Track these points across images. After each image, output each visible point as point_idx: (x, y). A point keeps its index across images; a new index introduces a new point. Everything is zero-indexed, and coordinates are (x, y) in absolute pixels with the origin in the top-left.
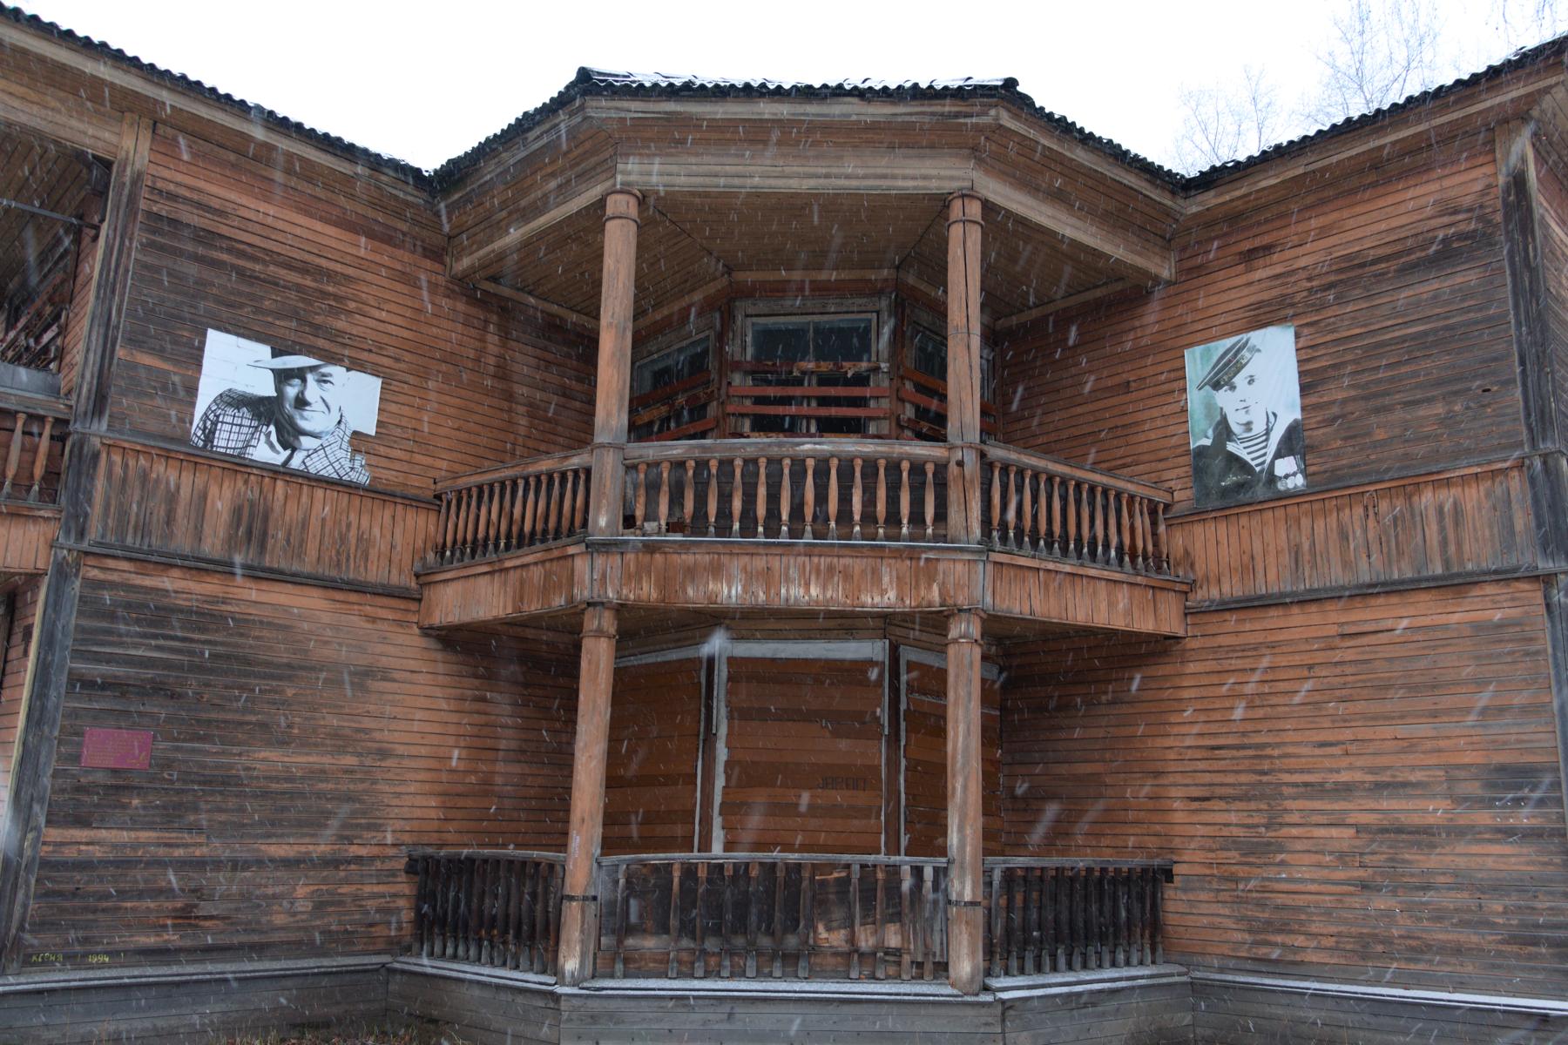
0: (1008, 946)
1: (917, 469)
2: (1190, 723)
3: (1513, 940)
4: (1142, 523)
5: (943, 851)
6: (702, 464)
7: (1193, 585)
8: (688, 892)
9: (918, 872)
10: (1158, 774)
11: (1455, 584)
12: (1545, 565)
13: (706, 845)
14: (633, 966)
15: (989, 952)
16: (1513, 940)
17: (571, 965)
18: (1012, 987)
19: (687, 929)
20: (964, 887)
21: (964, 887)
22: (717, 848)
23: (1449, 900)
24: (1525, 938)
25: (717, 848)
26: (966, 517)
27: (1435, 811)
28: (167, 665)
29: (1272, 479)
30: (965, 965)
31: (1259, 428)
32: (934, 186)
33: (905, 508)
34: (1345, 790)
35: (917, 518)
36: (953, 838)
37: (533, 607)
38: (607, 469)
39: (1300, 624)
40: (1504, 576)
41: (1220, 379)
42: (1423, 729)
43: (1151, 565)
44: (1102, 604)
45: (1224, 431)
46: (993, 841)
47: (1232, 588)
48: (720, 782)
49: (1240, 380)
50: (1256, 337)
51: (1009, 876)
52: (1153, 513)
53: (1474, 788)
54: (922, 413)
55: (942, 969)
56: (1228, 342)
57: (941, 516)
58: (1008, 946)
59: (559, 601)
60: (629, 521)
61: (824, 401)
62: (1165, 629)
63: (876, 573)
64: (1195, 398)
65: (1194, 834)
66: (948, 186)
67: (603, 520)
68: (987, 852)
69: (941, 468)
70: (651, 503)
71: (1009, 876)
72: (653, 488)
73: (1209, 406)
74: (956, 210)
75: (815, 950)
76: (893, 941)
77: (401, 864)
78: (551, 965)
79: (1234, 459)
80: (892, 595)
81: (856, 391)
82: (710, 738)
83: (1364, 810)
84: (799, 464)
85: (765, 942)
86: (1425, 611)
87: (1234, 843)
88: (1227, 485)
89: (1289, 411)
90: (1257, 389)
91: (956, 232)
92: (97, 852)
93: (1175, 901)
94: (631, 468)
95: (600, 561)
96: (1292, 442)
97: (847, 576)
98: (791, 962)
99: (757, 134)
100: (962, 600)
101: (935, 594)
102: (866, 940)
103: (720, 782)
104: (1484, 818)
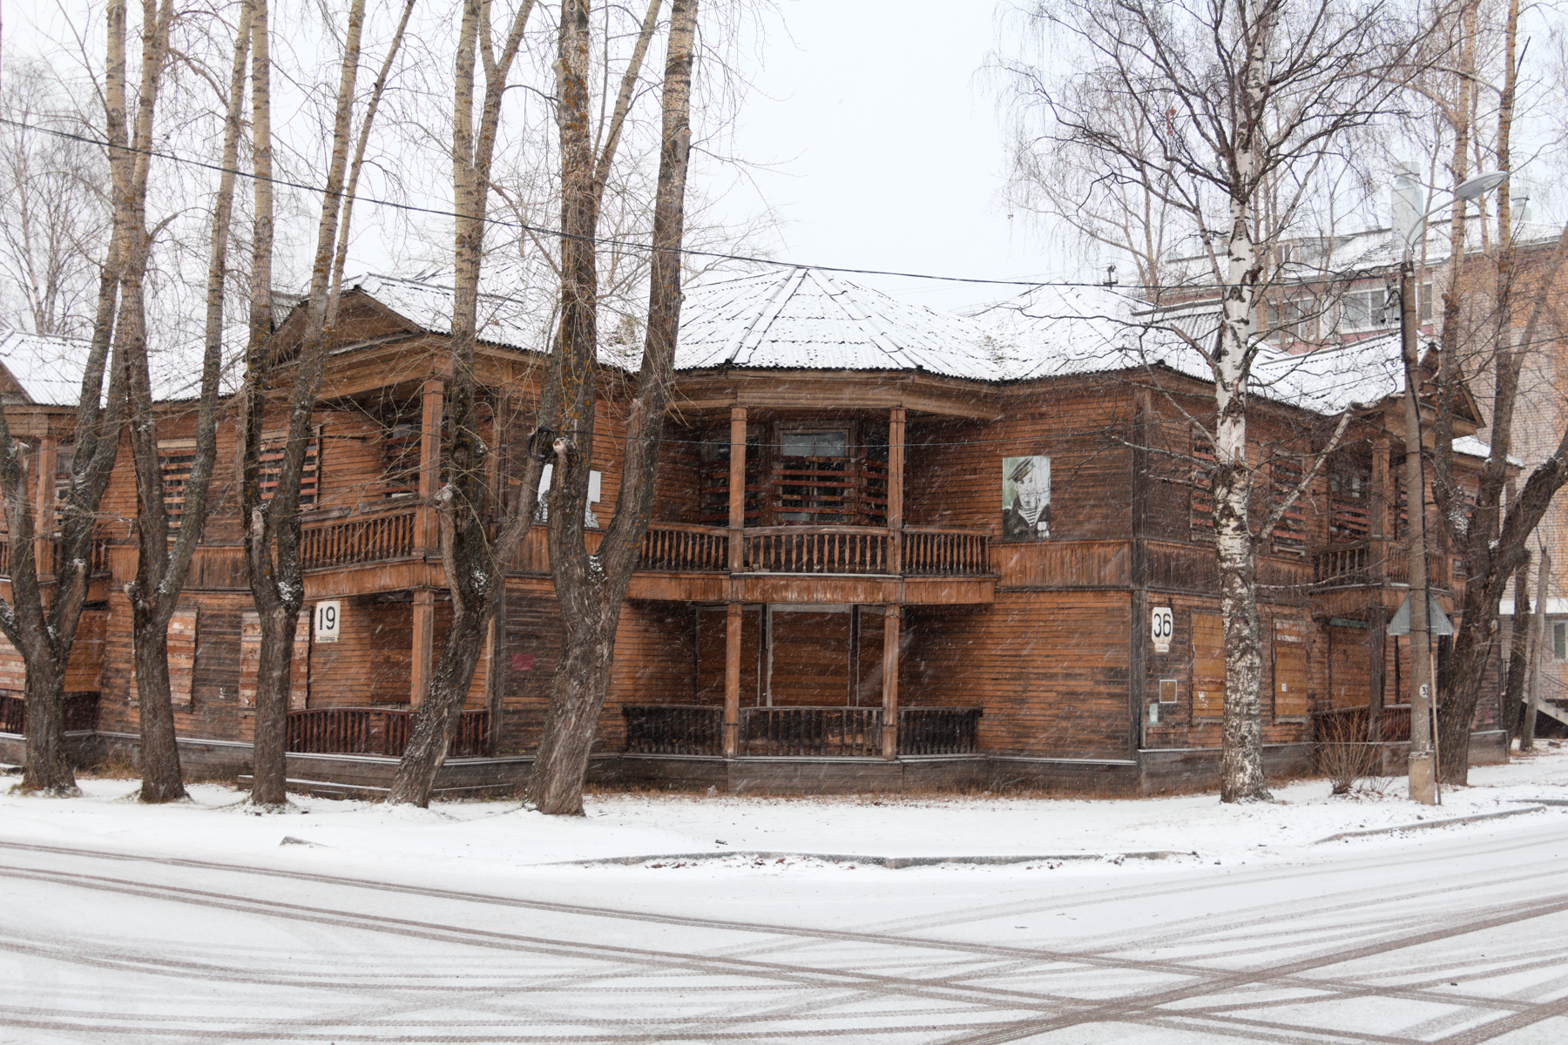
0: (908, 741)
1: (874, 538)
2: (999, 640)
3: (1108, 737)
4: (977, 549)
5: (880, 704)
6: (779, 537)
7: (999, 578)
8: (776, 723)
9: (870, 713)
10: (978, 667)
11: (1101, 590)
12: (1132, 586)
13: (763, 703)
14: (754, 751)
15: (898, 745)
16: (1108, 737)
17: (730, 751)
18: (908, 759)
19: (776, 737)
20: (889, 719)
21: (889, 719)
22: (769, 704)
23: (1088, 722)
24: (1113, 736)
25: (769, 704)
26: (895, 561)
27: (1083, 685)
28: (533, 624)
29: (1036, 532)
30: (889, 748)
31: (1033, 505)
32: (884, 405)
33: (868, 554)
34: (1053, 676)
35: (873, 561)
36: (885, 700)
37: (698, 598)
38: (737, 542)
39: (1046, 601)
40: (1117, 589)
41: (1018, 477)
42: (1085, 652)
43: (982, 570)
44: (950, 592)
45: (1017, 503)
46: (903, 697)
47: (1014, 582)
48: (770, 673)
49: (1026, 479)
50: (1036, 459)
51: (908, 714)
52: (983, 544)
53: (1100, 677)
54: (872, 482)
55: (879, 752)
56: (1022, 459)
57: (884, 561)
58: (908, 741)
59: (712, 598)
60: (746, 563)
61: (821, 479)
62: (985, 601)
63: (855, 588)
64: (1007, 484)
65: (992, 692)
66: (890, 404)
67: (736, 564)
68: (899, 704)
69: (884, 539)
70: (756, 555)
71: (908, 714)
72: (756, 548)
73: (1012, 490)
74: (893, 417)
75: (828, 745)
76: (860, 741)
77: (620, 711)
78: (720, 749)
79: (1021, 519)
80: (862, 597)
81: (840, 473)
82: (765, 651)
83: (1061, 685)
84: (822, 537)
85: (807, 741)
86: (1090, 600)
87: (1010, 700)
88: (1015, 531)
89: (1045, 501)
90: (1031, 484)
91: (893, 426)
92: (519, 707)
93: (982, 726)
94: (746, 539)
95: (736, 583)
96: (1047, 515)
97: (843, 589)
98: (818, 750)
99: (803, 384)
100: (892, 599)
101: (881, 597)
102: (848, 740)
103: (770, 673)
104: (1102, 688)
